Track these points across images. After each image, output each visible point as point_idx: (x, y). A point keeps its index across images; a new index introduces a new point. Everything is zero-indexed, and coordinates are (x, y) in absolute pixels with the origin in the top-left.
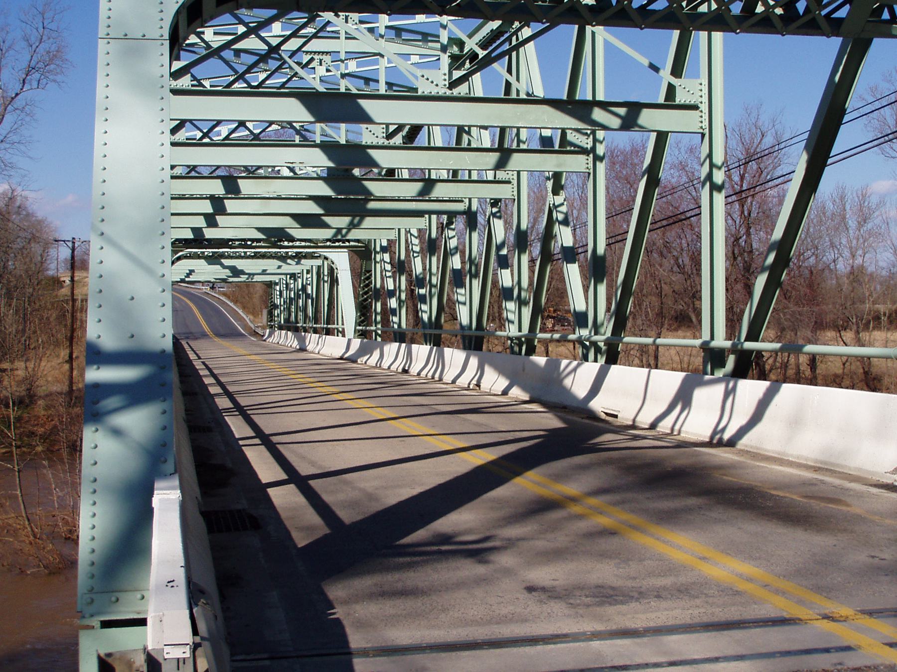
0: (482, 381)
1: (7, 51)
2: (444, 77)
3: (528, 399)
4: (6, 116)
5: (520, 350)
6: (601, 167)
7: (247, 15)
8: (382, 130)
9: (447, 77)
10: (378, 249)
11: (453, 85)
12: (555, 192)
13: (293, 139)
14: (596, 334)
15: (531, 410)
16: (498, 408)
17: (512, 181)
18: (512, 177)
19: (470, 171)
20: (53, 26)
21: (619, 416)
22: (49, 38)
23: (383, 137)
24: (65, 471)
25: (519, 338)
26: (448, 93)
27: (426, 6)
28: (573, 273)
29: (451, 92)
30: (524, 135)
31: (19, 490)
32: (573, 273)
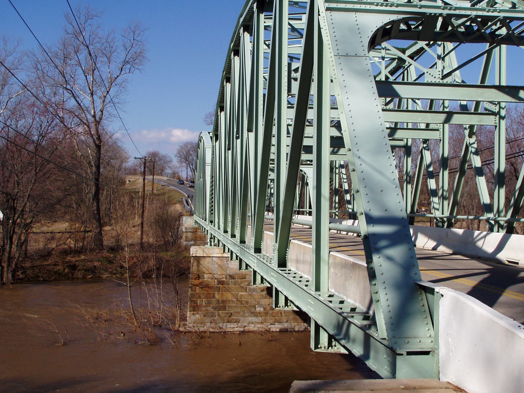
0: (417, 242)
1: (113, 52)
2: (439, 73)
3: (451, 253)
4: (111, 88)
5: (443, 226)
6: (503, 123)
7: (292, 35)
8: (383, 101)
9: (441, 73)
10: (337, 166)
11: (444, 77)
12: (470, 136)
13: (336, 107)
14: (499, 216)
15: (460, 259)
16: (438, 257)
17: (439, 129)
18: (439, 127)
19: (407, 123)
20: (139, 39)
21: (519, 262)
22: (137, 45)
23: (383, 104)
24: (154, 287)
25: (441, 218)
26: (441, 81)
27: (485, 38)
28: (482, 182)
29: (442, 81)
30: (447, 103)
31: (130, 297)
32: (482, 182)
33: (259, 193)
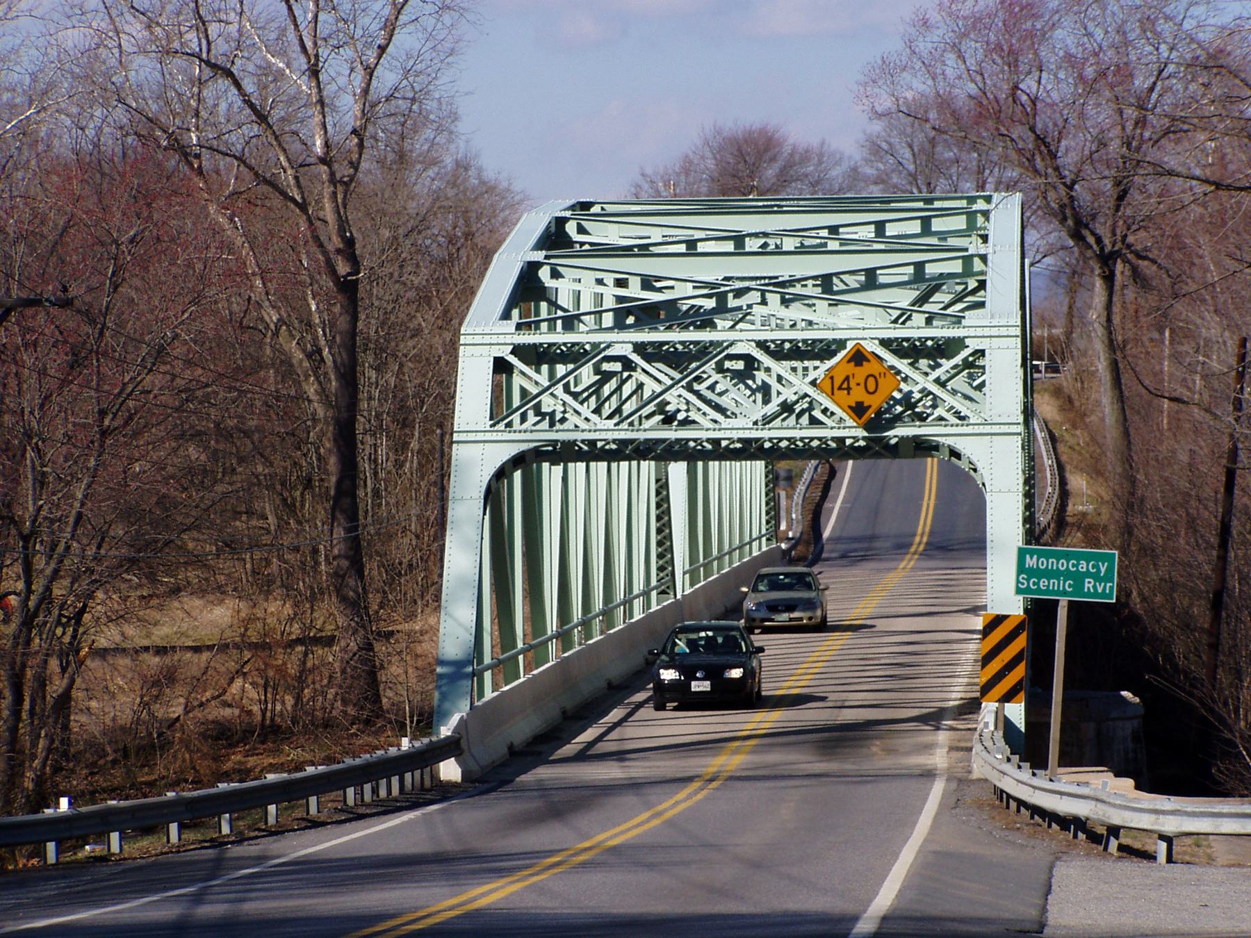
33: (370, 834)
